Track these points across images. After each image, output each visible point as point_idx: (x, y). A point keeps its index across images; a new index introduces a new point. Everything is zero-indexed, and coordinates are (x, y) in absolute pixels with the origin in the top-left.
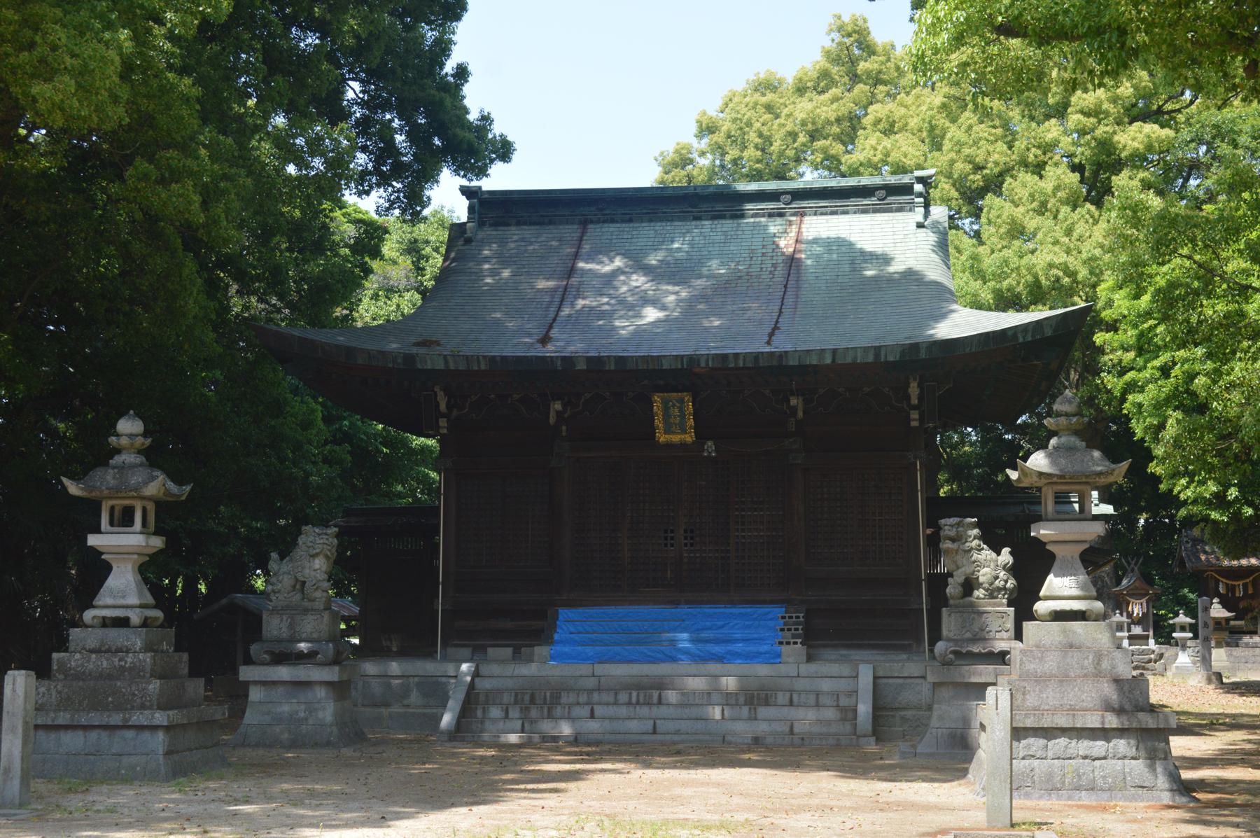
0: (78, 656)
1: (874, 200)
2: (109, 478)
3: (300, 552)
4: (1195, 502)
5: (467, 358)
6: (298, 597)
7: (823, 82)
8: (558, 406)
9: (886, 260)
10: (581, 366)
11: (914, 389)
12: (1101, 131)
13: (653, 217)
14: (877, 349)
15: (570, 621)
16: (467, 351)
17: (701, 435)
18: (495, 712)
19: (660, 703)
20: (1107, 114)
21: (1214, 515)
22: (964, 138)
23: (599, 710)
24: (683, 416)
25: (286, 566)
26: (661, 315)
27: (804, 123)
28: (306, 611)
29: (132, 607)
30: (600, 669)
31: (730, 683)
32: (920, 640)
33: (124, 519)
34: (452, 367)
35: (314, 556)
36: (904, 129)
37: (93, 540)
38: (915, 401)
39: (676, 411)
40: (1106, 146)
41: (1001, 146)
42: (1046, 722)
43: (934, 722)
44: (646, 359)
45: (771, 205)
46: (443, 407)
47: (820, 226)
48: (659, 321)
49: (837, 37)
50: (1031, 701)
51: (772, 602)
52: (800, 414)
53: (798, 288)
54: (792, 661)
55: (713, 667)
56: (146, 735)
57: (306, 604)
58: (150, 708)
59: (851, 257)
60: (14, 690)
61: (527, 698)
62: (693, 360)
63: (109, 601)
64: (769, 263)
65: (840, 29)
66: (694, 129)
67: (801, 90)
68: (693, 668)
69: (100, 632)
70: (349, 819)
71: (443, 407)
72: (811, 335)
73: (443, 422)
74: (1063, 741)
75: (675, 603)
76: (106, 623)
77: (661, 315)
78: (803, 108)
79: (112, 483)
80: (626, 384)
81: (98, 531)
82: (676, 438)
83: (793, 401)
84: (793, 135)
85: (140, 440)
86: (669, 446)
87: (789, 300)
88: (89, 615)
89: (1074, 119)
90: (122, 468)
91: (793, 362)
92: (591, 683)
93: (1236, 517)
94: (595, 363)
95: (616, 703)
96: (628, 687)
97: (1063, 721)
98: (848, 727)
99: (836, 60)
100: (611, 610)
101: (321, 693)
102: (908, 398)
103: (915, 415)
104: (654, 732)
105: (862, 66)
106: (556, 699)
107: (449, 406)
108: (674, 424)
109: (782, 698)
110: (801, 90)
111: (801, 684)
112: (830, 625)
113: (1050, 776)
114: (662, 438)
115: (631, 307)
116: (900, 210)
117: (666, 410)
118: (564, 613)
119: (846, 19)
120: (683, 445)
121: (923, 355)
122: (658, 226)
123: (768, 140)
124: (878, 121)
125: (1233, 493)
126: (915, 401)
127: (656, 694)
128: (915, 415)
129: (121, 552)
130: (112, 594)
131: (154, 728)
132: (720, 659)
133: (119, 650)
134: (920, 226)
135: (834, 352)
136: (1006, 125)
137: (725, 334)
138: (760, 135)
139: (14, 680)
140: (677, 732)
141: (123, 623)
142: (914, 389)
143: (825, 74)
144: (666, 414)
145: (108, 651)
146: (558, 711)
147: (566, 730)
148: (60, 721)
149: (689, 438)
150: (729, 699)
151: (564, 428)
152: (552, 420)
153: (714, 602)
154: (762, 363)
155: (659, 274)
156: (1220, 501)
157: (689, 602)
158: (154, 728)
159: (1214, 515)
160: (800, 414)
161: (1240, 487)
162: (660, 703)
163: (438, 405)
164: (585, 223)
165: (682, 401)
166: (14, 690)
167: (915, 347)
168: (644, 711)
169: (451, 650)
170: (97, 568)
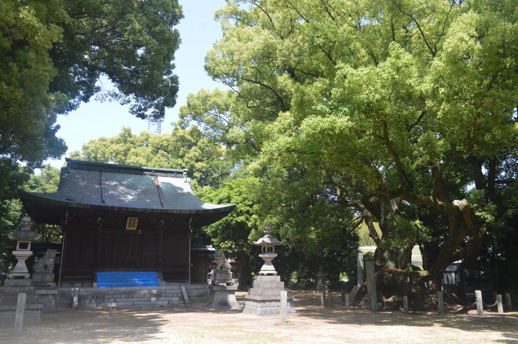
0: (8, 288)
1: (174, 175)
2: (22, 234)
3: (46, 257)
4: (224, 248)
5: (84, 205)
6: (44, 269)
7: (118, 142)
8: (100, 219)
9: (183, 189)
10: (116, 209)
11: (190, 220)
12: (192, 163)
13: (119, 172)
14: (190, 210)
15: (100, 275)
16: (84, 202)
17: (138, 228)
18: (87, 301)
19: (132, 297)
20: (193, 159)
21: (229, 251)
22: (158, 160)
23: (117, 300)
24: (134, 223)
25: (41, 260)
26: (132, 197)
27: (115, 151)
28: (47, 274)
29: (26, 273)
30: (114, 289)
31: (155, 291)
32: (188, 280)
33: (24, 246)
34: (79, 206)
35: (50, 258)
36: (140, 155)
37: (14, 253)
38: (190, 223)
39: (133, 222)
40: (193, 166)
41: (166, 163)
42: (271, 299)
43: (215, 300)
44: (133, 209)
45: (149, 173)
46: (67, 217)
47: (162, 180)
48: (132, 199)
49: (124, 132)
50: (266, 294)
51: (153, 271)
52: (163, 224)
53: (162, 194)
54: (164, 287)
55: (150, 288)
56: (35, 312)
57: (47, 271)
58: (35, 303)
59: (175, 189)
60: (22, 299)
61: (95, 297)
62: (145, 210)
63: (18, 271)
64: (152, 187)
65: (124, 129)
66: (81, 148)
67: (112, 142)
68: (144, 288)
69: (15, 281)
70: (140, 331)
71: (67, 217)
72: (169, 206)
73: (66, 221)
74: (273, 303)
75: (128, 271)
76: (16, 278)
77: (132, 197)
78: (115, 147)
79: (24, 236)
80: (124, 213)
81: (15, 250)
82: (131, 229)
83: (162, 221)
84: (111, 153)
85: (31, 223)
86: (129, 230)
87: (161, 197)
88: (260, 272)
89: (186, 159)
90: (26, 231)
91: (170, 212)
92: (113, 292)
93: (234, 251)
94: (120, 209)
95: (120, 298)
96: (124, 293)
97: (274, 298)
98: (182, 302)
99: (122, 136)
100: (113, 273)
101: (51, 297)
102: (189, 222)
103: (190, 226)
104: (133, 305)
105: (129, 139)
106: (104, 298)
107: (68, 217)
108: (132, 225)
109: (164, 295)
110: (112, 142)
111: (167, 291)
112: (172, 275)
113: (271, 311)
114: (127, 228)
115: (123, 195)
116: (180, 178)
117: (130, 221)
118: (98, 274)
119: (126, 127)
120: (133, 230)
121: (200, 213)
122: (121, 174)
123: (104, 153)
124: (133, 153)
125: (234, 246)
126: (190, 223)
127: (131, 295)
128: (190, 226)
129: (22, 256)
130: (18, 268)
131: (37, 309)
132: (151, 285)
133: (22, 286)
134: (186, 182)
135: (180, 210)
136: (168, 158)
137: (151, 203)
138: (102, 152)
139: (22, 297)
140: (139, 305)
141: (22, 278)
142: (190, 220)
143: (120, 139)
144: (130, 223)
145: (18, 286)
146: (106, 300)
147: (114, 305)
148: (5, 309)
149: (134, 229)
150: (156, 296)
151: (454, 294)
152: (98, 222)
153: (138, 271)
154: (162, 212)
155: (128, 186)
156: (230, 248)
157: (131, 271)
158: (37, 309)
159: (229, 251)
160: (163, 224)
161: (235, 245)
162: (132, 297)
163: (65, 216)
164: (101, 171)
165: (135, 219)
166: (22, 299)
167: (199, 211)
168: (130, 299)
169: (63, 284)
170: (14, 260)
